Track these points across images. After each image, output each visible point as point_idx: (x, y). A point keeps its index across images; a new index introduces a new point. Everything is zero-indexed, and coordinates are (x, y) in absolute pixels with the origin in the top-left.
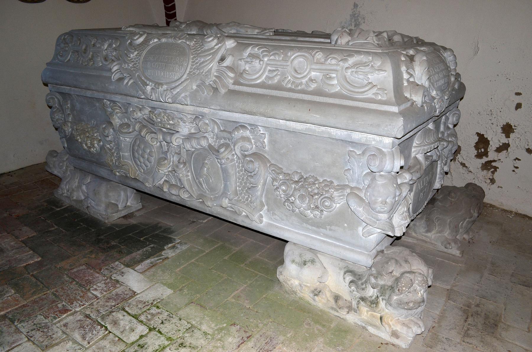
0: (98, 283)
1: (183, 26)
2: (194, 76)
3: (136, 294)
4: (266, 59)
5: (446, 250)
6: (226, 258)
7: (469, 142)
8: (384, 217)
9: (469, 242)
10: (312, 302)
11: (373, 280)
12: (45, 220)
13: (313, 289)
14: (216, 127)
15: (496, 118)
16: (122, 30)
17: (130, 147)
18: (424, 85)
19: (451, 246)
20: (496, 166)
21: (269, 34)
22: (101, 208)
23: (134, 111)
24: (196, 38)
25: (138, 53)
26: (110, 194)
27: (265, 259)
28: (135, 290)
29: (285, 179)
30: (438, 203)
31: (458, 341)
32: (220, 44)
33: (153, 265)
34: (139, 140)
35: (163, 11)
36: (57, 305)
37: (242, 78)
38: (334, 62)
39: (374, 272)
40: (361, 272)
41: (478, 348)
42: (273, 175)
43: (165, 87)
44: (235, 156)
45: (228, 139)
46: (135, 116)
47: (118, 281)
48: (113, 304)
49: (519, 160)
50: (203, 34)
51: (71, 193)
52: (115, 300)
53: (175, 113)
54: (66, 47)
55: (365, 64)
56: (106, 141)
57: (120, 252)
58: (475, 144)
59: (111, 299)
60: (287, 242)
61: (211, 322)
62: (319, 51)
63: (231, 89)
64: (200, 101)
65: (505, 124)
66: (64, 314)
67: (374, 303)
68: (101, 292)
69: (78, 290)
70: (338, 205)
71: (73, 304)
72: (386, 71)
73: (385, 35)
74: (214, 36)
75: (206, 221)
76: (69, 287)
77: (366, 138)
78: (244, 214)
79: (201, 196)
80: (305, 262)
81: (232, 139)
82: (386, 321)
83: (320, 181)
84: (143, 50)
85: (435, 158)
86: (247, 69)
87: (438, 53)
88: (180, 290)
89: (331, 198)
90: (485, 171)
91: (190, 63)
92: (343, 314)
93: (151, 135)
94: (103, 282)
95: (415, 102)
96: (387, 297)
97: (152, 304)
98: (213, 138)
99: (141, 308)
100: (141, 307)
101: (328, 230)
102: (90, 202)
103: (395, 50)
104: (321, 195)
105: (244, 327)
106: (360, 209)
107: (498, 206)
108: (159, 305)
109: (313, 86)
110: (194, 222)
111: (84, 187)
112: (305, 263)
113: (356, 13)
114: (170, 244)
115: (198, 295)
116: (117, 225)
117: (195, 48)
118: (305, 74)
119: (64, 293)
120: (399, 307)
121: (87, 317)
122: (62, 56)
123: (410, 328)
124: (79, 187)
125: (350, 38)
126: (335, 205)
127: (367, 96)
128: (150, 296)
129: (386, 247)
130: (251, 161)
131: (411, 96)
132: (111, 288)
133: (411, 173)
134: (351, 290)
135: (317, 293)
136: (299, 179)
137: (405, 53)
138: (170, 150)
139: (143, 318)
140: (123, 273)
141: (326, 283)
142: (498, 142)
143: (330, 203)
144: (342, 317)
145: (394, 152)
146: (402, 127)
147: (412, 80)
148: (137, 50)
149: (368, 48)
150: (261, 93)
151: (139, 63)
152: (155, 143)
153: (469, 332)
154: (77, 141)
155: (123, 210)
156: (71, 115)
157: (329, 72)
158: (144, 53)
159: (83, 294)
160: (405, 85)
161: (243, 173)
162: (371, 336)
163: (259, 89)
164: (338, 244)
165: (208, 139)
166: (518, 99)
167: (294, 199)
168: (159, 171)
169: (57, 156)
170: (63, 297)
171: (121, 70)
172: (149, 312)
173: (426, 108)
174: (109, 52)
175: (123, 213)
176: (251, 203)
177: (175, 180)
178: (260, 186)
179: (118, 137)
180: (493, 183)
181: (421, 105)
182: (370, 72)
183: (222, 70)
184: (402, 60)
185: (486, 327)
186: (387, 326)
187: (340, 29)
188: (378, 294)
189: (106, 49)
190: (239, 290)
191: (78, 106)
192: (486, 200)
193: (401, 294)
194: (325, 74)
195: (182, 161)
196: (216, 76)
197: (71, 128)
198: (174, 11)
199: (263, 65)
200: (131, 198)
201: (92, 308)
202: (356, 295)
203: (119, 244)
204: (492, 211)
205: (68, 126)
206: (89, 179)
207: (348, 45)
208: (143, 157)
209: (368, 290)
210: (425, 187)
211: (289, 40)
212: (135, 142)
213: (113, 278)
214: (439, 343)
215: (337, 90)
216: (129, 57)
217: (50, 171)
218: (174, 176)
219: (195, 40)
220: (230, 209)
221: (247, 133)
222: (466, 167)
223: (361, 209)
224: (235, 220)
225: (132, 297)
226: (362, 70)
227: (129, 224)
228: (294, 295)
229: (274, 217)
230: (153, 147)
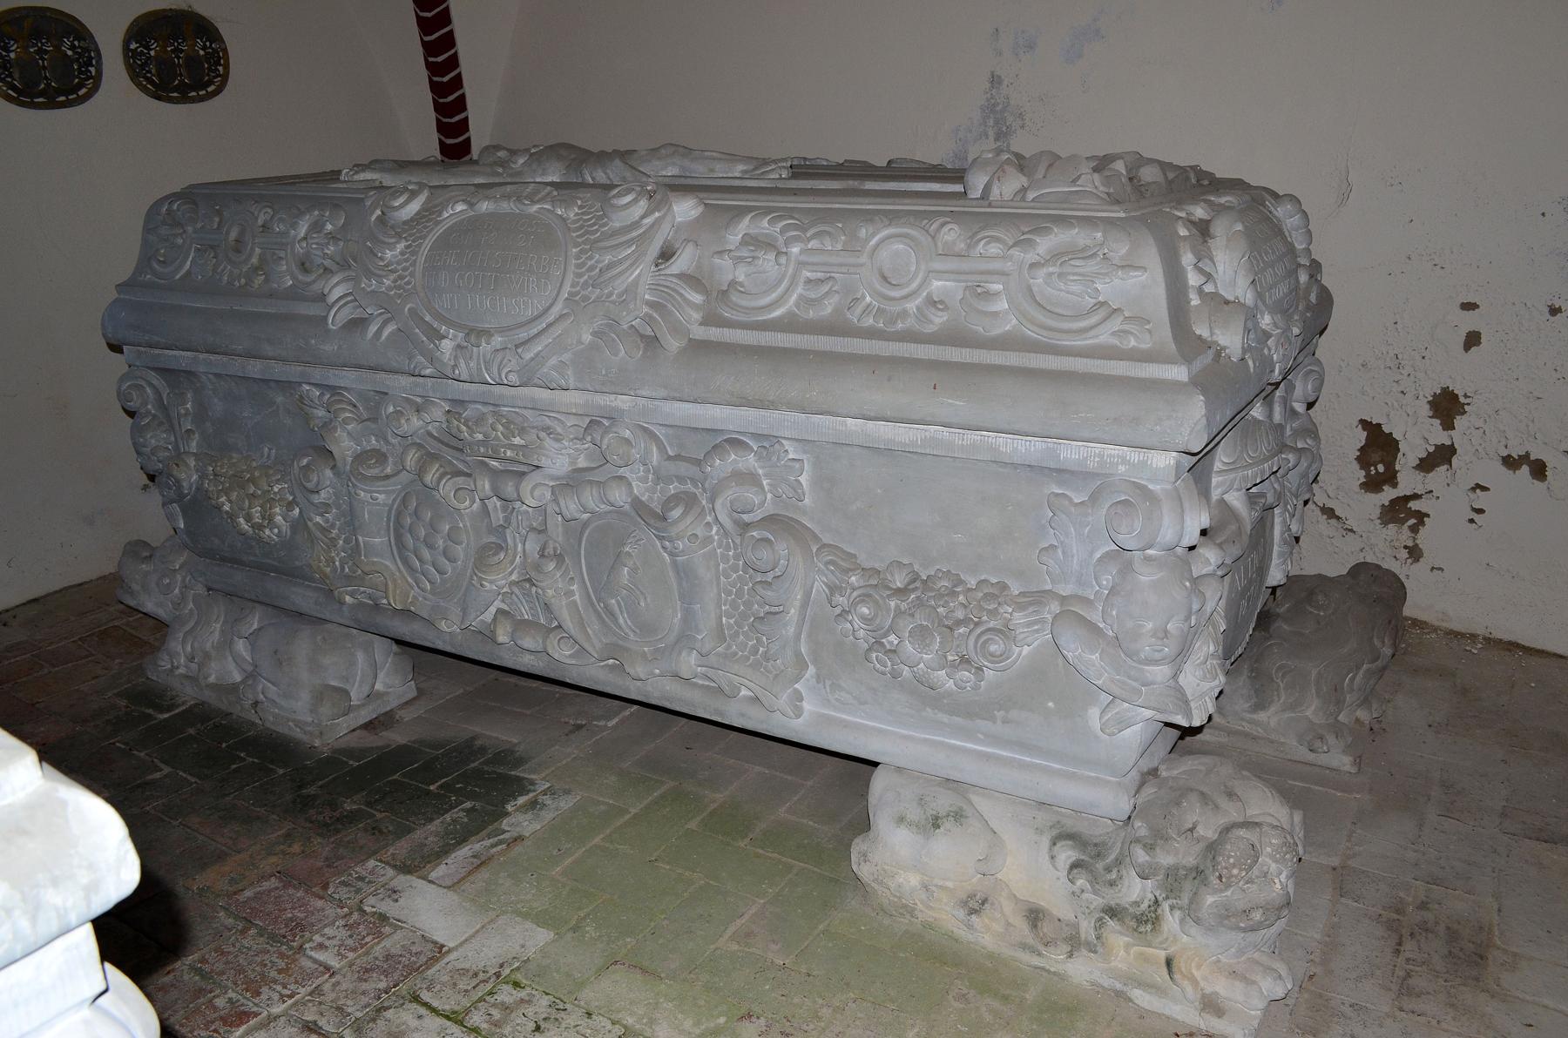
0: (325, 926)
1: (521, 161)
2: (583, 304)
3: (444, 950)
4: (795, 250)
5: (1311, 757)
6: (693, 825)
7: (1341, 446)
8: (1160, 672)
9: (1372, 729)
10: (962, 933)
11: (1141, 855)
12: (130, 749)
13: (964, 897)
14: (655, 449)
15: (1412, 377)
16: (342, 178)
17: (389, 520)
18: (1242, 301)
19: (1327, 744)
21: (778, 176)
22: (299, 704)
23: (399, 413)
24: (581, 196)
25: (407, 247)
26: (327, 661)
27: (805, 821)
28: (441, 940)
29: (866, 586)
30: (1282, 626)
31: (1386, 1009)
32: (659, 211)
33: (481, 862)
34: (417, 499)
35: (431, 116)
36: (211, 1001)
37: (728, 306)
38: (994, 249)
39: (1143, 832)
40: (1100, 836)
41: (1444, 1025)
42: (831, 576)
43: (498, 340)
44: (715, 529)
45: (692, 480)
46: (405, 428)
47: (383, 918)
48: (382, 985)
49: (1484, 489)
50: (580, 180)
51: (201, 666)
52: (386, 973)
53: (525, 412)
54: (175, 236)
55: (1085, 254)
56: (312, 504)
57: (375, 830)
58: (1358, 454)
59: (372, 970)
60: (875, 764)
61: (680, 1016)
62: (949, 219)
63: (697, 337)
64: (606, 375)
66: (239, 1026)
67: (1146, 920)
68: (339, 954)
69: (268, 951)
70: (1026, 650)
71: (258, 994)
72: (1144, 269)
73: (1120, 166)
74: (638, 189)
76: (237, 945)
77: (1101, 456)
78: (744, 692)
79: (616, 652)
80: (937, 818)
81: (706, 479)
82: (1183, 969)
83: (969, 586)
84: (424, 238)
85: (1270, 499)
86: (741, 278)
87: (1261, 208)
88: (575, 929)
89: (1006, 632)
90: (1390, 526)
91: (571, 268)
92: (1055, 959)
93: (455, 479)
94: (340, 923)
95: (1224, 348)
96: (1186, 901)
97: (498, 977)
98: (644, 480)
99: (466, 991)
100: (465, 987)
101: (999, 722)
102: (263, 688)
103: (1156, 209)
104: (977, 624)
105: (778, 1022)
106: (1094, 657)
107: (1436, 623)
108: (519, 977)
109: (938, 321)
110: (579, 727)
111: (241, 646)
112: (936, 823)
113: (998, 101)
114: (519, 795)
115: (629, 940)
116: (350, 752)
117: (581, 227)
118: (914, 285)
119: (227, 963)
120: (1224, 926)
121: (311, 1030)
122: (164, 262)
123: (1254, 983)
124: (226, 644)
125: (1024, 181)
126: (1018, 649)
127: (1096, 341)
128: (489, 951)
129: (1163, 761)
130: (767, 540)
131: (1212, 334)
132: (367, 940)
133: (1220, 546)
134: (1075, 888)
135: (976, 906)
136: (909, 584)
137: (1183, 215)
138: (514, 520)
139: (476, 1019)
140: (395, 892)
141: (999, 876)
142: (1422, 442)
143: (1002, 646)
144: (1052, 969)
145: (1181, 491)
146: (1204, 421)
147: (1209, 288)
148: (405, 238)
149: (1082, 206)
150: (787, 345)
151: (412, 275)
152: (467, 503)
153: (1410, 981)
154: (219, 508)
155: (363, 705)
156: (197, 435)
157: (983, 278)
158: (427, 244)
159: (287, 964)
160: (1193, 303)
161: (739, 577)
162: (1142, 1017)
163: (779, 335)
164: (1028, 759)
165: (630, 484)
166: (1469, 322)
167: (896, 642)
168: (481, 585)
169: (151, 556)
170: (225, 977)
171: (357, 298)
172: (492, 1000)
173: (1250, 363)
174: (314, 246)
175: (365, 715)
176: (768, 660)
177: (531, 608)
178: (793, 611)
179: (353, 491)
180: (1417, 560)
181: (1240, 357)
182: (1101, 274)
183: (668, 284)
184: (1181, 237)
185: (1455, 964)
186: (1186, 982)
187: (990, 155)
188: (1157, 895)
189: (305, 238)
190: (747, 917)
191: (218, 407)
192: (1408, 611)
193: (1228, 886)
194: (969, 284)
195: (552, 553)
196: (651, 305)
197: (197, 471)
198: (462, 116)
199: (787, 266)
200: (386, 669)
201: (320, 1003)
202: (1091, 903)
203: (367, 806)
204: (1420, 638)
205: (187, 465)
206: (257, 618)
207: (1023, 199)
208: (431, 547)
209: (1126, 883)
210: (1250, 582)
211: (837, 190)
212: (404, 502)
213: (368, 909)
214: (1336, 1019)
215: (1006, 329)
216: (382, 259)
217: (132, 603)
218: (527, 595)
219: (579, 202)
220: (700, 682)
221: (750, 461)
222: (1338, 518)
223: (1095, 657)
224: (717, 712)
225: (433, 960)
226: (1076, 270)
227: (389, 746)
228: (908, 916)
230: (461, 516)
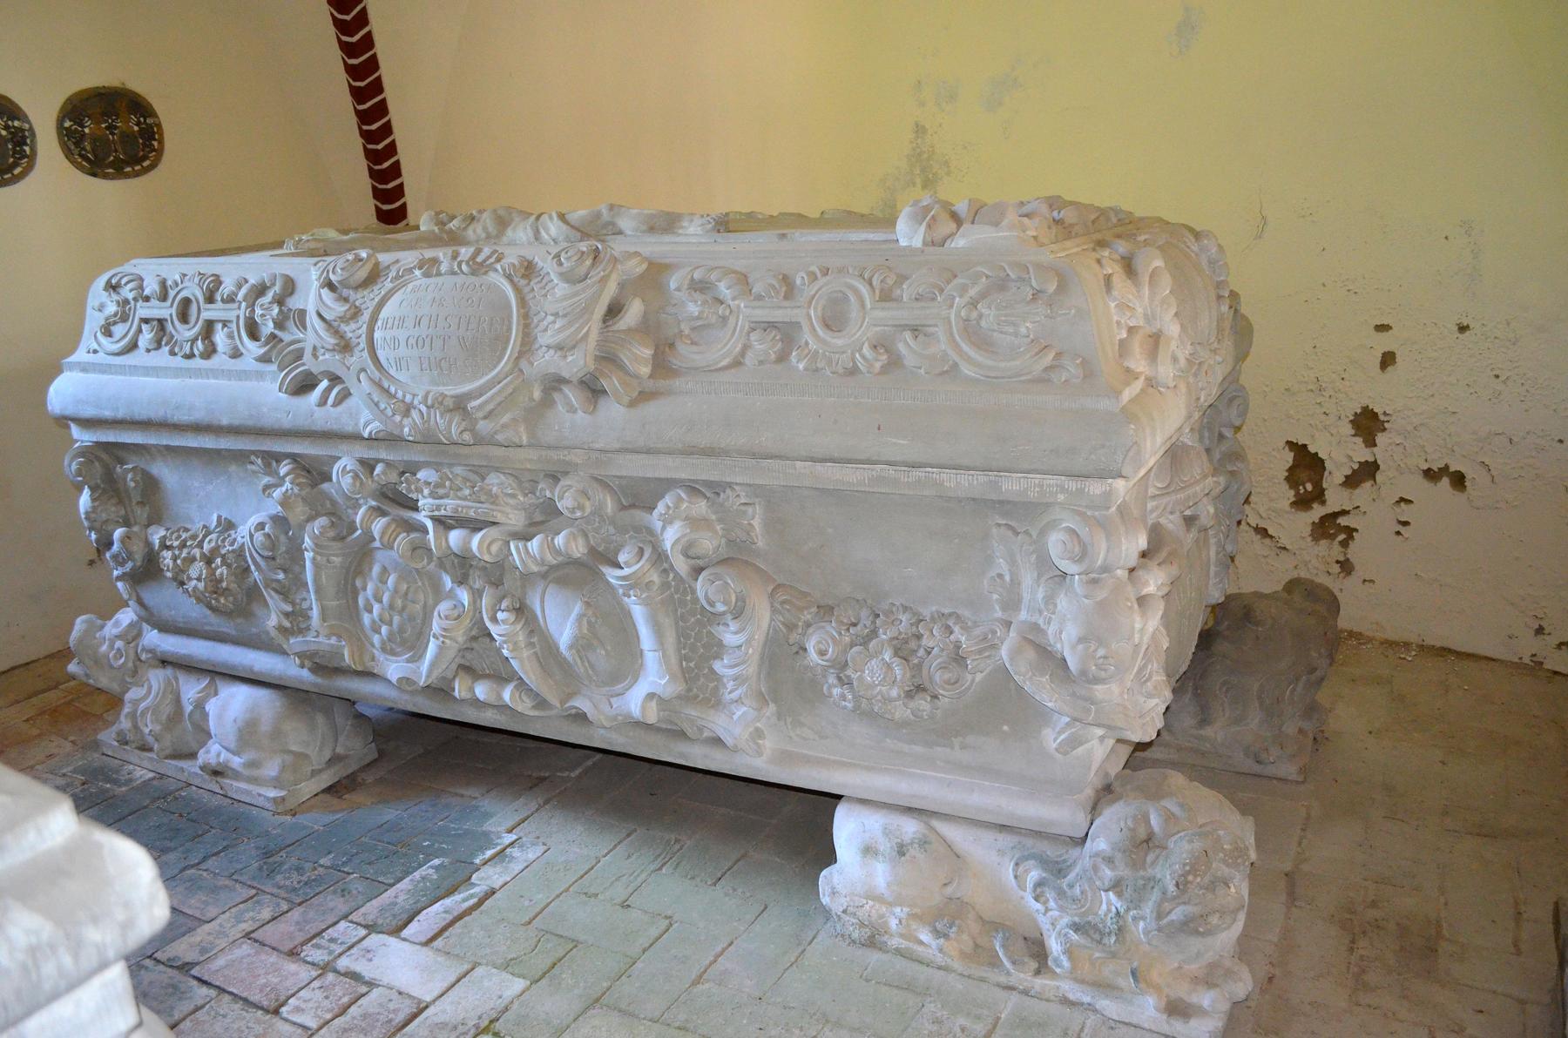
20: (1352, 526)
44: (671, 575)
60: (839, 797)
65: (1359, 411)
69: (245, 1018)
75: (577, 772)
101: (957, 747)
107: (1370, 634)
126: (969, 677)
140: (368, 951)
142: (1346, 460)
153: (1365, 978)
166: (1384, 343)
192: (1344, 622)
222: (1271, 537)
224: (682, 755)
229: (798, 732)
